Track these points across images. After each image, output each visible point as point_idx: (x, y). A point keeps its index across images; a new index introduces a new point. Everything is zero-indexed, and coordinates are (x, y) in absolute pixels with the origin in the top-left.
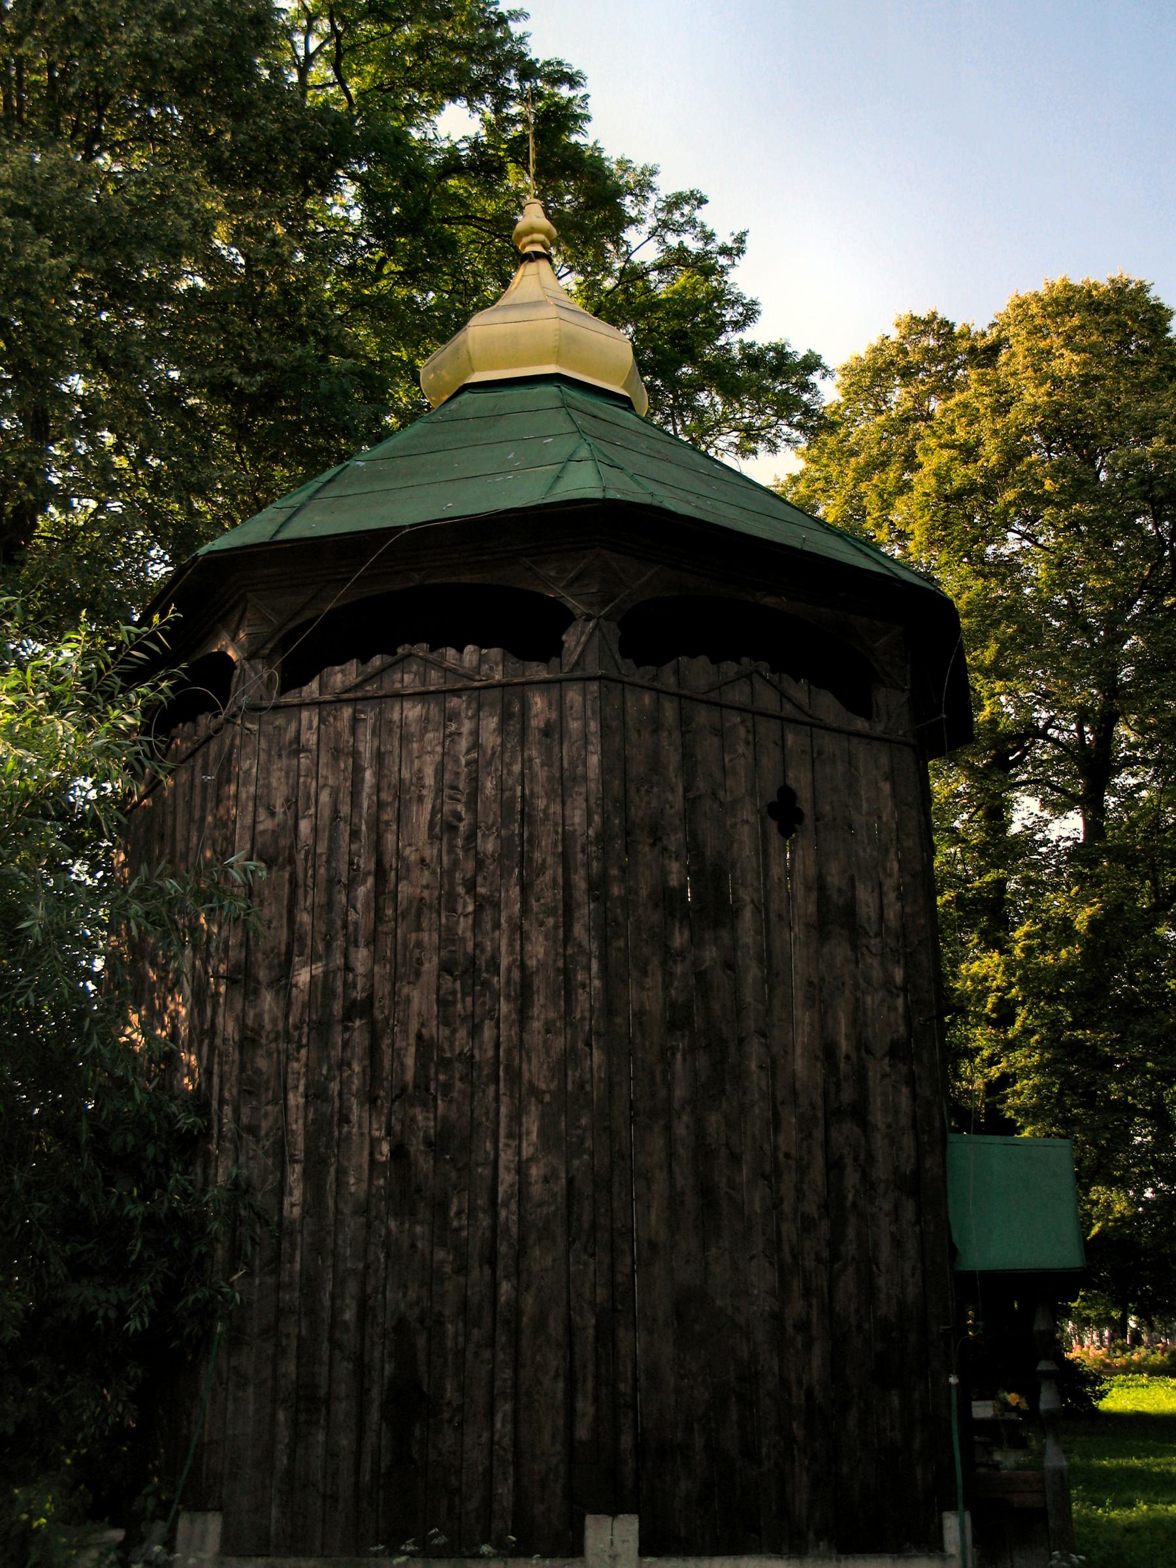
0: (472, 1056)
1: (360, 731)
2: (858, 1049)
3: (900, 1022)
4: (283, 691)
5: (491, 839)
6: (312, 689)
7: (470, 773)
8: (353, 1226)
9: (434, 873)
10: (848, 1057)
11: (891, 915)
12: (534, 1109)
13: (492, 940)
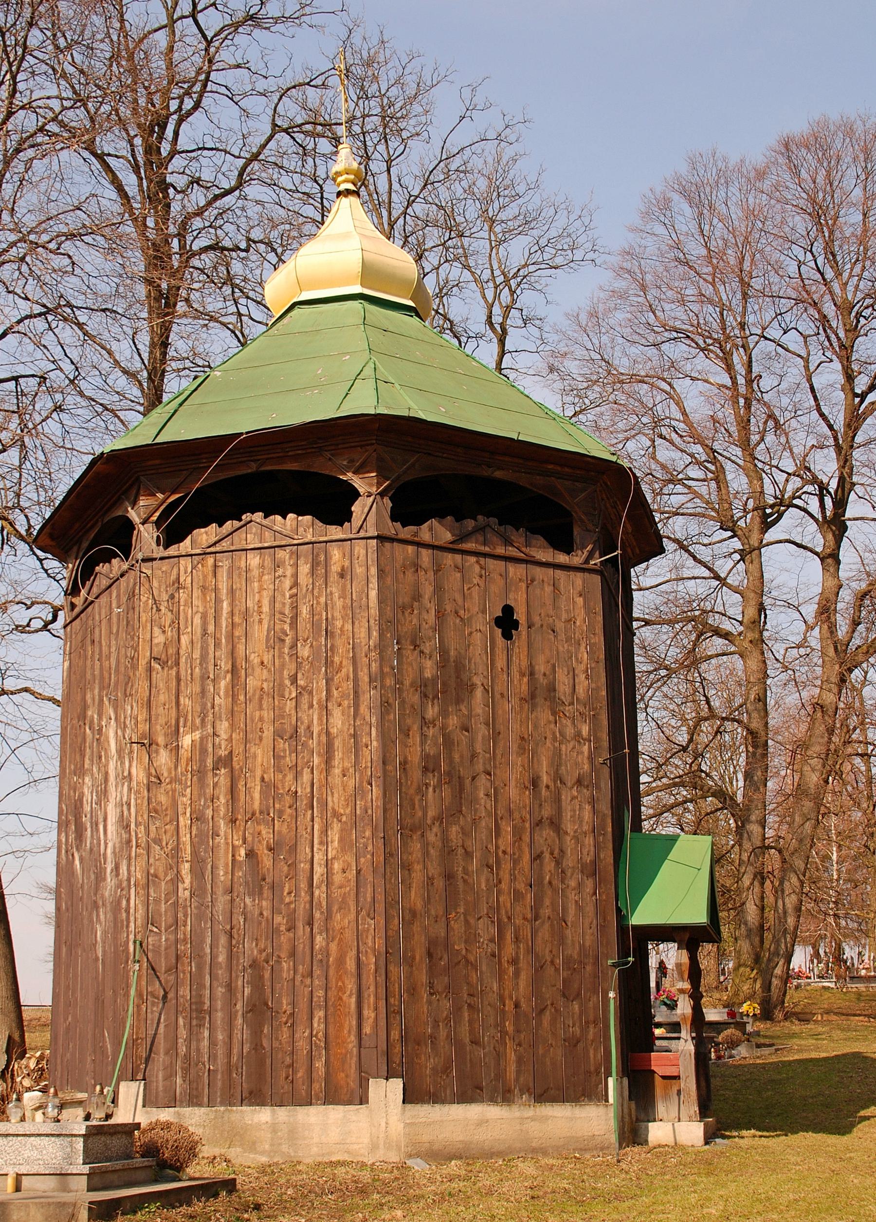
0: (296, 792)
1: (219, 575)
2: (555, 782)
3: (586, 761)
4: (166, 547)
5: (307, 647)
6: (186, 546)
7: (292, 603)
8: (222, 900)
9: (269, 671)
10: (547, 787)
11: (581, 691)
12: (336, 826)
13: (308, 715)
